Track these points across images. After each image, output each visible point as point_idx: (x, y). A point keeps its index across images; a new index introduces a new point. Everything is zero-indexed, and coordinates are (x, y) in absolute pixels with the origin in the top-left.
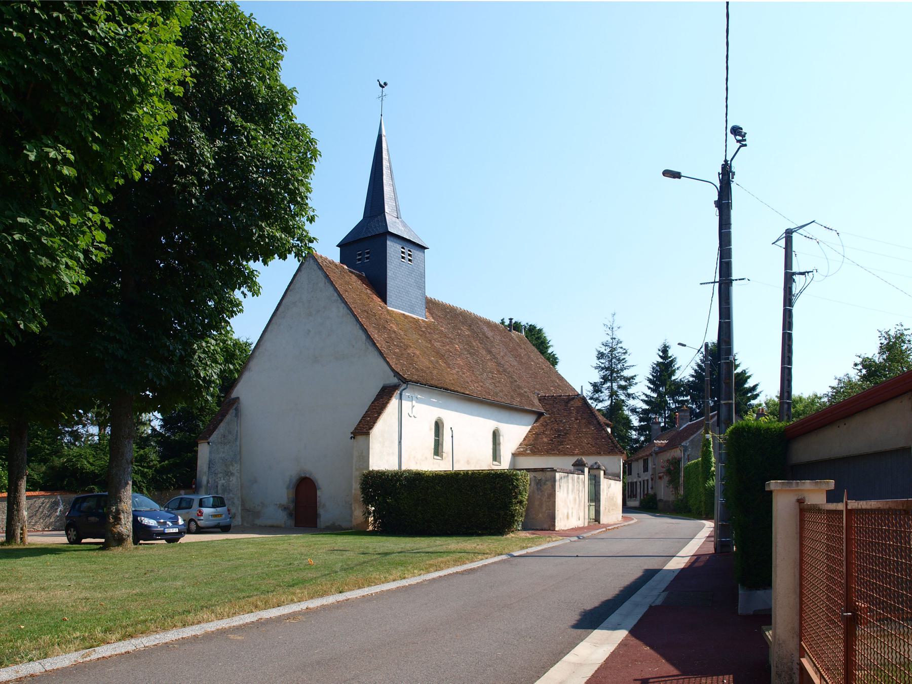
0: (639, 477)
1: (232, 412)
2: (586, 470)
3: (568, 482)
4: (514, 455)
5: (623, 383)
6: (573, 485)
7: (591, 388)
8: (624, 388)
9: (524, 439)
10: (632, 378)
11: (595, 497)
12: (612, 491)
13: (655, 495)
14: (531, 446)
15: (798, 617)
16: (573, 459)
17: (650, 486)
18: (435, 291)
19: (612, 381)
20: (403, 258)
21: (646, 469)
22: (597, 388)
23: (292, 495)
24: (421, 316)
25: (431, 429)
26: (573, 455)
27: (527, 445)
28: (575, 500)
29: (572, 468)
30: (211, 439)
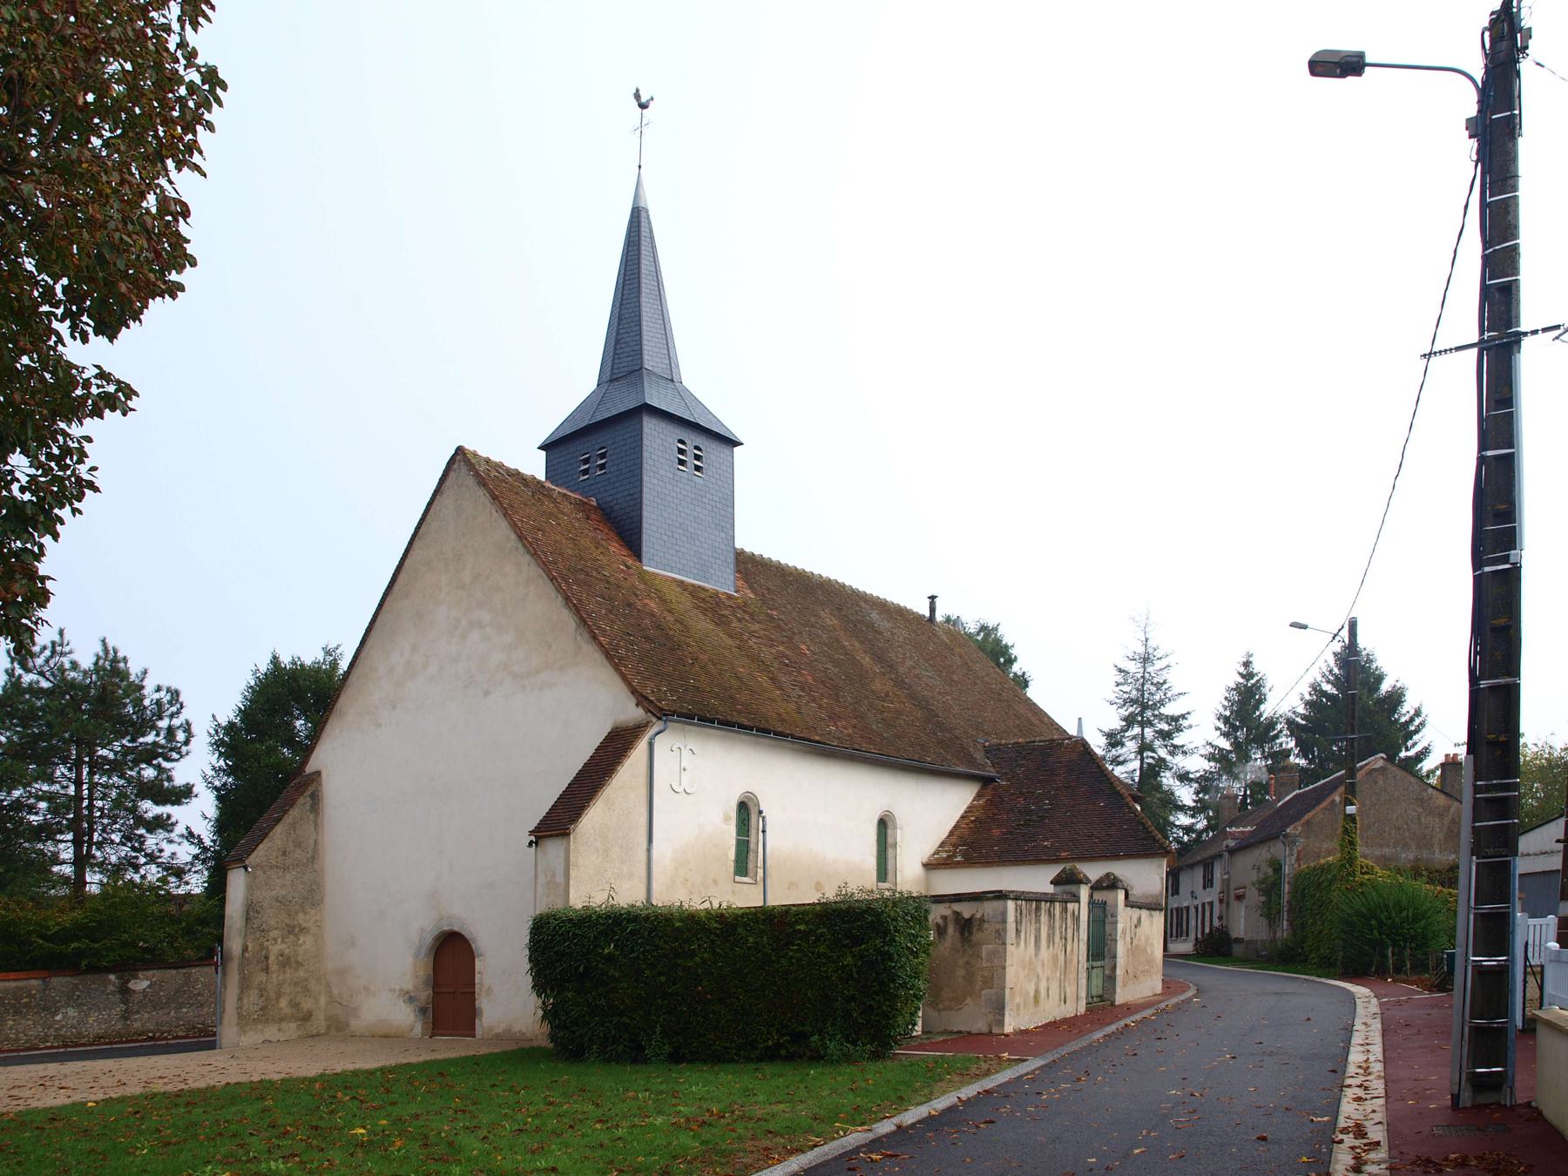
1: (304, 801)
2: (1084, 892)
3: (1038, 921)
4: (929, 866)
6: (1051, 927)
7: (1103, 741)
8: (1165, 735)
9: (951, 833)
10: (1183, 717)
11: (1100, 948)
12: (1142, 936)
14: (968, 845)
16: (1053, 871)
17: (1216, 913)
18: (753, 536)
19: (1143, 724)
20: (682, 462)
21: (1208, 882)
23: (425, 970)
24: (724, 582)
25: (727, 819)
26: (1057, 861)
28: (1055, 959)
29: (1050, 889)
30: (252, 859)
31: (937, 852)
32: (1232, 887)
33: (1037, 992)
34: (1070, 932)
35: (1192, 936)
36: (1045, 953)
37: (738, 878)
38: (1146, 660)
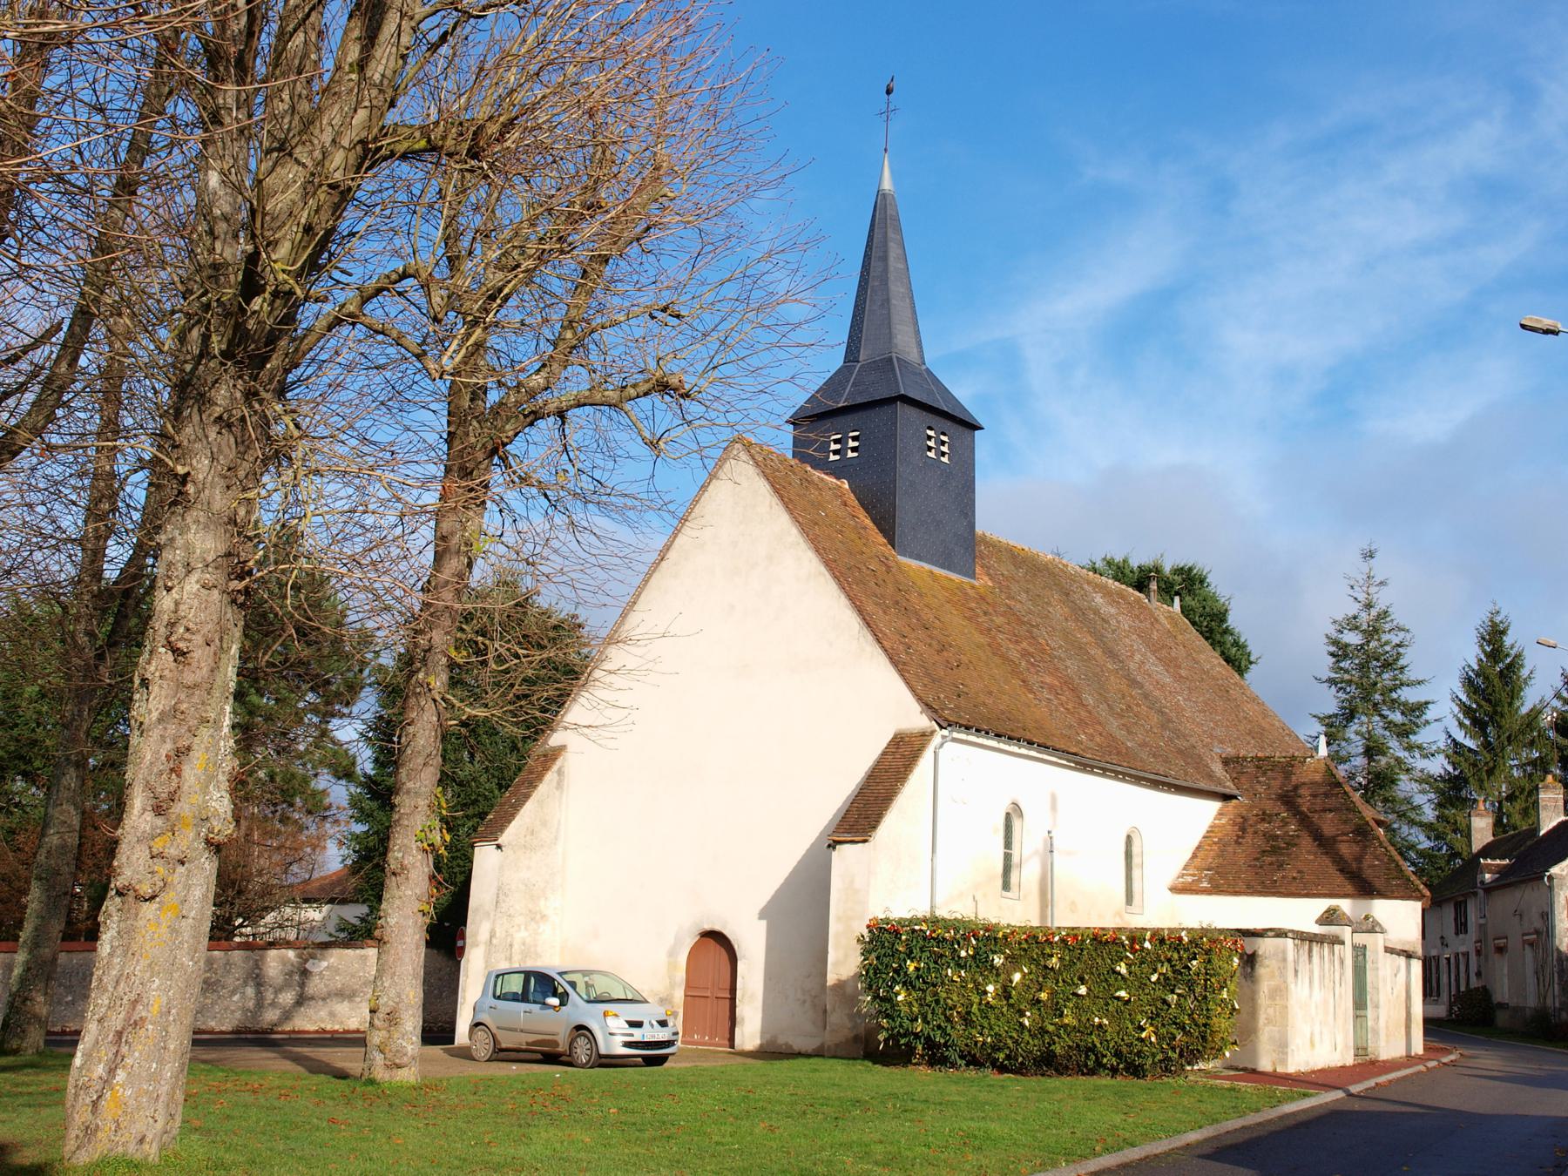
0: (1444, 944)
5: (1397, 717)
9: (1194, 856)
13: (1485, 993)
14: (1218, 870)
15: (653, 581)
16: (1321, 905)
17: (1473, 968)
21: (1461, 927)
22: (1334, 728)
35: (1445, 996)
38: (1372, 632)
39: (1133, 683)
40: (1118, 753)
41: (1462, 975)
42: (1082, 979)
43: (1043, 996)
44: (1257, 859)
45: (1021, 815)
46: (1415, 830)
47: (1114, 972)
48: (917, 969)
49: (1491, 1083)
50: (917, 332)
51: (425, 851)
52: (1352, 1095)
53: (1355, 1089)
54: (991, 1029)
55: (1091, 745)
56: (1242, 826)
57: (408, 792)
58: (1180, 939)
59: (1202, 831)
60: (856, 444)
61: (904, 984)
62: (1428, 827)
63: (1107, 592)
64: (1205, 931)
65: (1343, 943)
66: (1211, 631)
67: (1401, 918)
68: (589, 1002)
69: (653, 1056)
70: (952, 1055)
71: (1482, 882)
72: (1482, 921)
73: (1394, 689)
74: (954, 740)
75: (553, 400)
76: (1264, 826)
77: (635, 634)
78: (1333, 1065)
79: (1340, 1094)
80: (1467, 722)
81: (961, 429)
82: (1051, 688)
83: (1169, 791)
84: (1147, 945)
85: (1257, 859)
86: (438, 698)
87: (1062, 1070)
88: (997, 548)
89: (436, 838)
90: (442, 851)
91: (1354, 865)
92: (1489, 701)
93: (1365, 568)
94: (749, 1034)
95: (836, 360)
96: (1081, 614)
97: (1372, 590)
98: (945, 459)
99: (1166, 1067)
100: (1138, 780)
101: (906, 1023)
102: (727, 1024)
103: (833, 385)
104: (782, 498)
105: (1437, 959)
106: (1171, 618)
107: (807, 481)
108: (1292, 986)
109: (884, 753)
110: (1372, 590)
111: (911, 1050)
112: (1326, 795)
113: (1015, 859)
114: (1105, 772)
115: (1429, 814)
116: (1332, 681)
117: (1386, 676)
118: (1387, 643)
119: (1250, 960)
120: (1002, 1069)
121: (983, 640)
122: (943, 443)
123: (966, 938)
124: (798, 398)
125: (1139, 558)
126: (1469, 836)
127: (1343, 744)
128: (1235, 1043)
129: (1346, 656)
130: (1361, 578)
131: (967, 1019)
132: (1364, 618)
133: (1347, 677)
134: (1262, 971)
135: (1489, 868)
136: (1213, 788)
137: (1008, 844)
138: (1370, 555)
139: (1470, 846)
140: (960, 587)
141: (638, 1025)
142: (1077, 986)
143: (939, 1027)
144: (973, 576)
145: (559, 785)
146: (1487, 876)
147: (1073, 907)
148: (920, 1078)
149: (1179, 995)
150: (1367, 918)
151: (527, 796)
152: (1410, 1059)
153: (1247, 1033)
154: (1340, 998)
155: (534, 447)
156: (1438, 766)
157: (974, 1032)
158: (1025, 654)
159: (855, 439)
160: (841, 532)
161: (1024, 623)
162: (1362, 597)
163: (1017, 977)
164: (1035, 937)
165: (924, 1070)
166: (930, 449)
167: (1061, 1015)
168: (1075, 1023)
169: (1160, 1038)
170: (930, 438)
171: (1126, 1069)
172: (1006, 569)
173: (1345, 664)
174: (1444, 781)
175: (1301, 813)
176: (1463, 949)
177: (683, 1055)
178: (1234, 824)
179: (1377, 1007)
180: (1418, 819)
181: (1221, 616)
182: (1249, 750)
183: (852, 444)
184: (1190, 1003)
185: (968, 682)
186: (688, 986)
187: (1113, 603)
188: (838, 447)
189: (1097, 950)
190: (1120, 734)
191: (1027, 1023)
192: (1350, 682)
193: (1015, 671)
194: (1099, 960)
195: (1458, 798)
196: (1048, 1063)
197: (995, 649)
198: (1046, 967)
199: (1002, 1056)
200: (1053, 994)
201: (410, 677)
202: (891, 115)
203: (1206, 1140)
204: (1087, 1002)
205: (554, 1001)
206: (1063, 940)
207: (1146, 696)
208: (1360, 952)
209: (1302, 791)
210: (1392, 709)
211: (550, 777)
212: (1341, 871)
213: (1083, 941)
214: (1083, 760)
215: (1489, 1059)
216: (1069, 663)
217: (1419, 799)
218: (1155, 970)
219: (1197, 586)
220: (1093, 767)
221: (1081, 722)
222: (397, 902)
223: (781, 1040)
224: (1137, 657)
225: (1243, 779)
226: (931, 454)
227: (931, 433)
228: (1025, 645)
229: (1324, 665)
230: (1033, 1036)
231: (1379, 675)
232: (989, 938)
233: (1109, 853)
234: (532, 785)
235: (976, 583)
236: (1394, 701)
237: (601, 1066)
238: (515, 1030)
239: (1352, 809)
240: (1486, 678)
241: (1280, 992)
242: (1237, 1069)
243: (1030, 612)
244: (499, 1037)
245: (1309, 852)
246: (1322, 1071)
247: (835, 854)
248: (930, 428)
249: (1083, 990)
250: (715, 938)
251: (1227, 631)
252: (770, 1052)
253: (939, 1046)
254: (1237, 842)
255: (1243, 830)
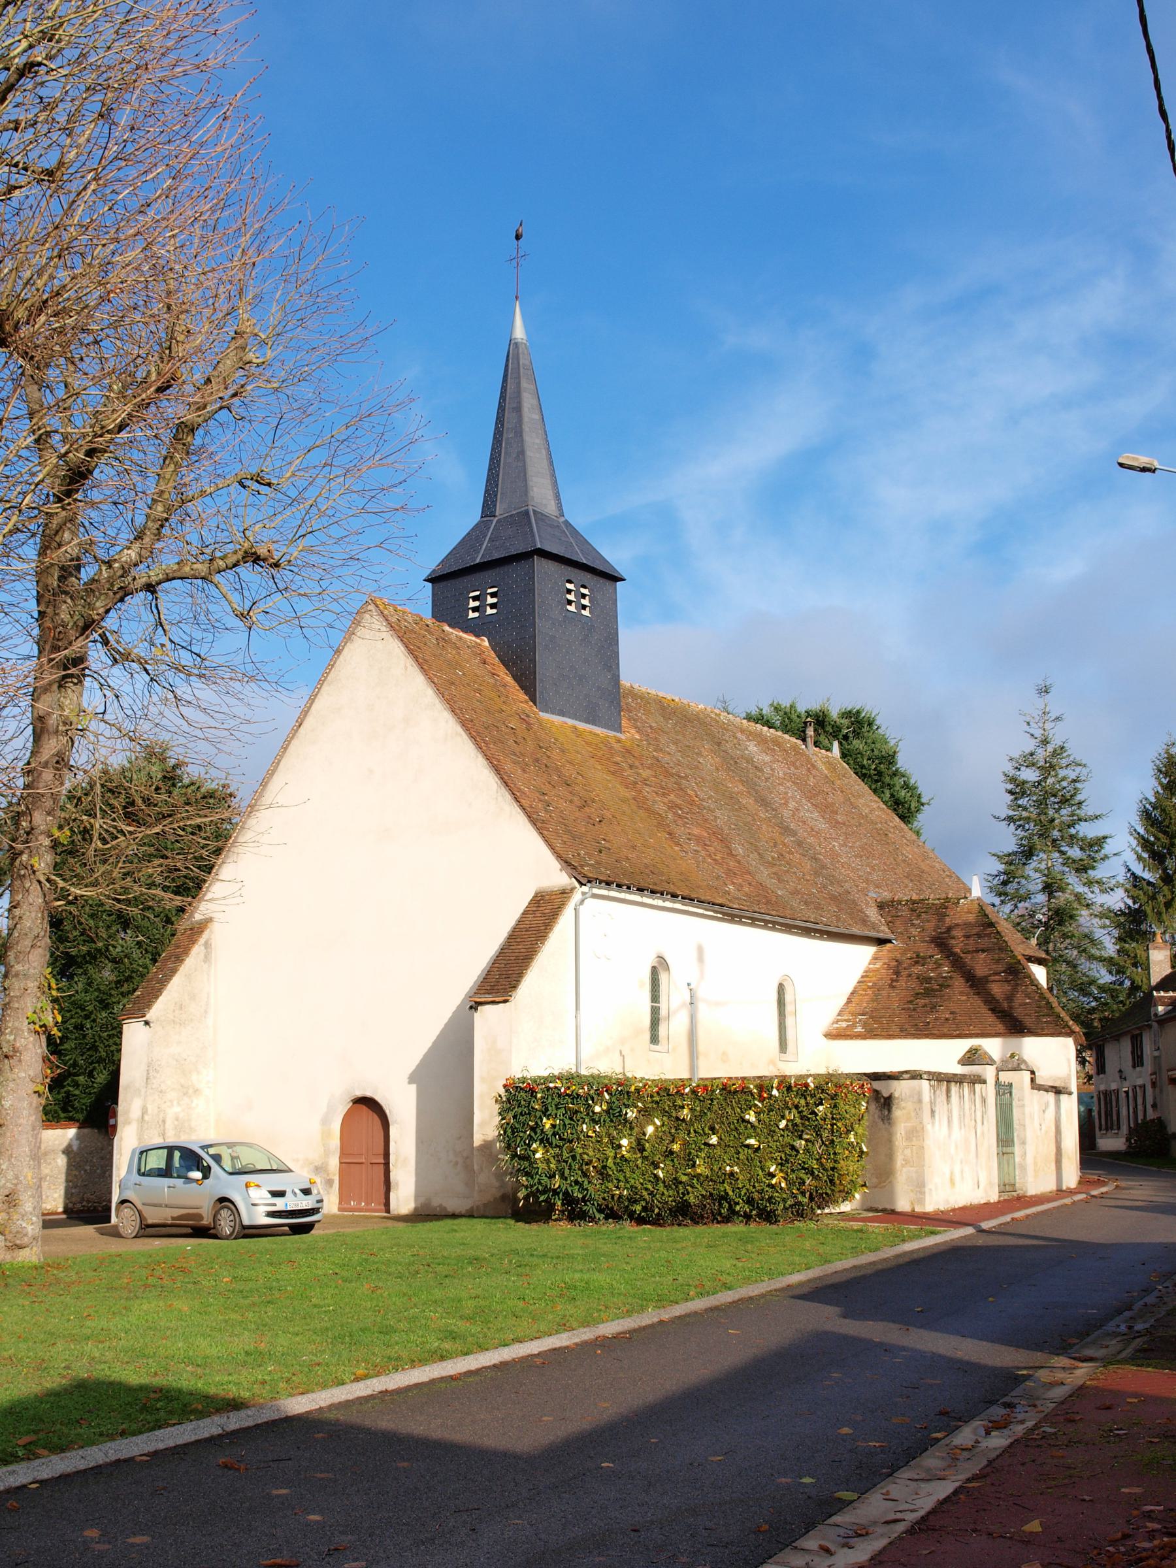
0: (1123, 1078)
5: (1075, 853)
9: (849, 1001)
13: (1160, 1124)
14: (872, 1015)
15: (292, 748)
16: (962, 1046)
21: (1138, 1061)
27: (854, 1014)
31: (837, 1022)
32: (1164, 1067)
33: (952, 1174)
34: (979, 1114)
35: (1124, 1129)
36: (957, 1133)
37: (653, 1047)
38: (1049, 768)
39: (787, 831)
40: (768, 902)
41: (1140, 1107)
42: (712, 1129)
43: (676, 1147)
44: (910, 1002)
45: (667, 968)
46: (1095, 965)
47: (744, 1121)
48: (553, 1126)
49: (1133, 1213)
50: (555, 484)
51: (37, 1032)
52: (983, 1231)
53: (986, 1225)
54: (627, 1182)
55: (739, 895)
56: (897, 970)
57: (17, 975)
58: (806, 1085)
59: (857, 976)
60: (495, 600)
61: (542, 1141)
62: (1109, 961)
63: (762, 740)
64: (829, 1077)
65: (985, 1082)
66: (880, 774)
67: (1055, 1056)
68: (231, 1174)
69: (299, 1224)
70: (591, 1209)
71: (1156, 1015)
72: (1156, 1054)
73: (1072, 825)
74: (595, 896)
75: (142, 575)
76: (917, 969)
77: (280, 799)
78: (975, 1202)
79: (970, 1230)
80: (1145, 855)
81: (602, 580)
82: (698, 839)
83: (821, 938)
84: (775, 1092)
85: (910, 1002)
86: (42, 879)
87: (697, 1219)
88: (645, 701)
89: (49, 1019)
90: (55, 1031)
91: (1005, 1004)
92: (1165, 833)
93: (1040, 703)
94: (404, 1199)
95: (473, 516)
96: (732, 763)
97: (1048, 726)
98: (586, 613)
99: (799, 1212)
100: (788, 928)
101: (545, 1180)
102: (382, 1190)
103: (471, 540)
104: (416, 658)
105: (1117, 1092)
106: (829, 763)
107: (444, 640)
108: (929, 1127)
109: (525, 913)
110: (1048, 726)
111: (551, 1207)
112: (979, 936)
113: (663, 1012)
114: (753, 922)
115: (1110, 948)
116: (1010, 819)
117: (1064, 812)
118: (1064, 779)
119: (886, 1103)
120: (640, 1221)
121: (629, 794)
122: (584, 596)
123: (600, 1094)
124: (433, 557)
125: (806, 703)
126: (1148, 969)
127: (1023, 881)
128: (864, 1185)
129: (1023, 794)
130: (1036, 713)
131: (603, 1173)
132: (1041, 755)
133: (1025, 814)
134: (897, 1113)
135: (1161, 1000)
136: (866, 933)
137: (655, 997)
138: (1046, 691)
139: (1149, 979)
140: (605, 741)
141: (280, 1194)
142: (708, 1135)
143: (576, 1182)
144: (619, 729)
145: (207, 958)
146: (1160, 1008)
147: (725, 1057)
148: (559, 1234)
149: (807, 1140)
150: (1012, 1056)
151: (174, 971)
152: (1060, 1193)
153: (884, 1175)
154: (988, 1136)
155: (129, 622)
156: (1117, 900)
157: (610, 1185)
158: (672, 806)
159: (493, 595)
160: (479, 691)
161: (671, 775)
162: (1038, 733)
163: (650, 1130)
164: (667, 1090)
165: (565, 1225)
166: (570, 602)
167: (694, 1166)
168: (708, 1172)
169: (790, 1184)
170: (569, 591)
171: (759, 1215)
172: (655, 721)
173: (1023, 802)
174: (1123, 913)
175: (954, 954)
176: (1139, 1082)
177: (333, 1220)
178: (889, 968)
179: (1024, 1143)
180: (1098, 953)
181: (889, 759)
182: (906, 893)
183: (490, 600)
184: (818, 1148)
185: (610, 837)
186: (343, 1153)
187: (768, 750)
188: (477, 604)
189: (727, 1099)
190: (770, 883)
191: (661, 1176)
192: (1028, 819)
193: (661, 824)
194: (729, 1110)
195: (1138, 932)
196: (683, 1213)
197: (641, 803)
198: (677, 1119)
199: (638, 1208)
200: (686, 1144)
201: (13, 860)
202: (522, 261)
203: (809, 1281)
204: (718, 1151)
205: (197, 1175)
206: (694, 1092)
207: (799, 844)
208: (1004, 1091)
209: (954, 933)
210: (1071, 845)
211: (197, 950)
212: (993, 1010)
213: (713, 1091)
214: (730, 911)
215: (1142, 1189)
216: (718, 813)
217: (1099, 933)
218: (783, 1117)
219: (866, 728)
220: (741, 917)
221: (730, 873)
222: (11, 1085)
223: (436, 1202)
224: (792, 804)
225: (898, 922)
226: (572, 608)
227: (570, 586)
228: (672, 797)
229: (1002, 803)
230: (667, 1187)
231: (1057, 811)
232: (622, 1092)
233: (762, 1001)
234: (179, 959)
235: (622, 736)
236: (1072, 837)
237: (245, 1236)
238: (160, 1206)
239: (1004, 947)
240: (1163, 810)
241: (916, 1133)
242: (877, 1211)
243: (679, 764)
244: (145, 1214)
245: (961, 993)
246: (963, 1209)
247: (477, 1016)
248: (570, 582)
249: (714, 1140)
250: (368, 1104)
251: (895, 774)
252: (423, 1215)
253: (577, 1201)
254: (891, 986)
255: (897, 973)
